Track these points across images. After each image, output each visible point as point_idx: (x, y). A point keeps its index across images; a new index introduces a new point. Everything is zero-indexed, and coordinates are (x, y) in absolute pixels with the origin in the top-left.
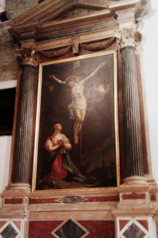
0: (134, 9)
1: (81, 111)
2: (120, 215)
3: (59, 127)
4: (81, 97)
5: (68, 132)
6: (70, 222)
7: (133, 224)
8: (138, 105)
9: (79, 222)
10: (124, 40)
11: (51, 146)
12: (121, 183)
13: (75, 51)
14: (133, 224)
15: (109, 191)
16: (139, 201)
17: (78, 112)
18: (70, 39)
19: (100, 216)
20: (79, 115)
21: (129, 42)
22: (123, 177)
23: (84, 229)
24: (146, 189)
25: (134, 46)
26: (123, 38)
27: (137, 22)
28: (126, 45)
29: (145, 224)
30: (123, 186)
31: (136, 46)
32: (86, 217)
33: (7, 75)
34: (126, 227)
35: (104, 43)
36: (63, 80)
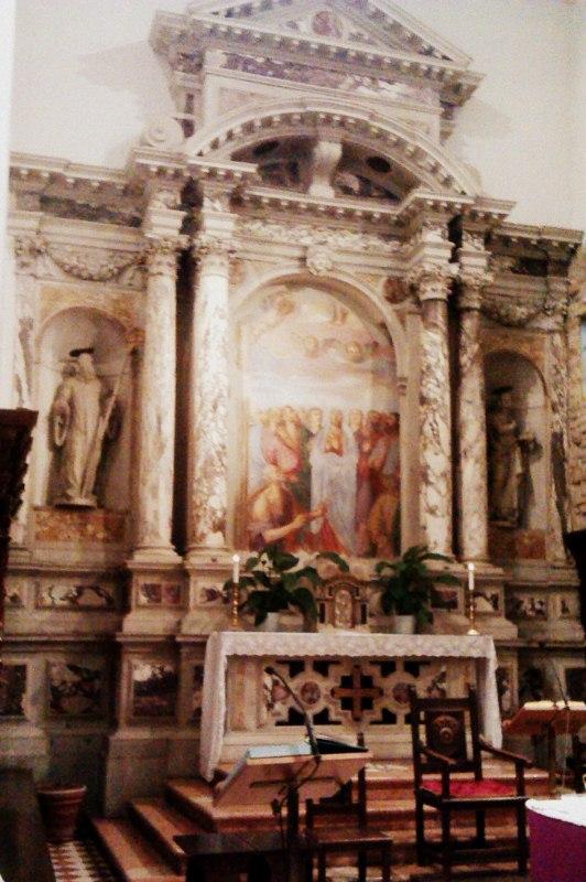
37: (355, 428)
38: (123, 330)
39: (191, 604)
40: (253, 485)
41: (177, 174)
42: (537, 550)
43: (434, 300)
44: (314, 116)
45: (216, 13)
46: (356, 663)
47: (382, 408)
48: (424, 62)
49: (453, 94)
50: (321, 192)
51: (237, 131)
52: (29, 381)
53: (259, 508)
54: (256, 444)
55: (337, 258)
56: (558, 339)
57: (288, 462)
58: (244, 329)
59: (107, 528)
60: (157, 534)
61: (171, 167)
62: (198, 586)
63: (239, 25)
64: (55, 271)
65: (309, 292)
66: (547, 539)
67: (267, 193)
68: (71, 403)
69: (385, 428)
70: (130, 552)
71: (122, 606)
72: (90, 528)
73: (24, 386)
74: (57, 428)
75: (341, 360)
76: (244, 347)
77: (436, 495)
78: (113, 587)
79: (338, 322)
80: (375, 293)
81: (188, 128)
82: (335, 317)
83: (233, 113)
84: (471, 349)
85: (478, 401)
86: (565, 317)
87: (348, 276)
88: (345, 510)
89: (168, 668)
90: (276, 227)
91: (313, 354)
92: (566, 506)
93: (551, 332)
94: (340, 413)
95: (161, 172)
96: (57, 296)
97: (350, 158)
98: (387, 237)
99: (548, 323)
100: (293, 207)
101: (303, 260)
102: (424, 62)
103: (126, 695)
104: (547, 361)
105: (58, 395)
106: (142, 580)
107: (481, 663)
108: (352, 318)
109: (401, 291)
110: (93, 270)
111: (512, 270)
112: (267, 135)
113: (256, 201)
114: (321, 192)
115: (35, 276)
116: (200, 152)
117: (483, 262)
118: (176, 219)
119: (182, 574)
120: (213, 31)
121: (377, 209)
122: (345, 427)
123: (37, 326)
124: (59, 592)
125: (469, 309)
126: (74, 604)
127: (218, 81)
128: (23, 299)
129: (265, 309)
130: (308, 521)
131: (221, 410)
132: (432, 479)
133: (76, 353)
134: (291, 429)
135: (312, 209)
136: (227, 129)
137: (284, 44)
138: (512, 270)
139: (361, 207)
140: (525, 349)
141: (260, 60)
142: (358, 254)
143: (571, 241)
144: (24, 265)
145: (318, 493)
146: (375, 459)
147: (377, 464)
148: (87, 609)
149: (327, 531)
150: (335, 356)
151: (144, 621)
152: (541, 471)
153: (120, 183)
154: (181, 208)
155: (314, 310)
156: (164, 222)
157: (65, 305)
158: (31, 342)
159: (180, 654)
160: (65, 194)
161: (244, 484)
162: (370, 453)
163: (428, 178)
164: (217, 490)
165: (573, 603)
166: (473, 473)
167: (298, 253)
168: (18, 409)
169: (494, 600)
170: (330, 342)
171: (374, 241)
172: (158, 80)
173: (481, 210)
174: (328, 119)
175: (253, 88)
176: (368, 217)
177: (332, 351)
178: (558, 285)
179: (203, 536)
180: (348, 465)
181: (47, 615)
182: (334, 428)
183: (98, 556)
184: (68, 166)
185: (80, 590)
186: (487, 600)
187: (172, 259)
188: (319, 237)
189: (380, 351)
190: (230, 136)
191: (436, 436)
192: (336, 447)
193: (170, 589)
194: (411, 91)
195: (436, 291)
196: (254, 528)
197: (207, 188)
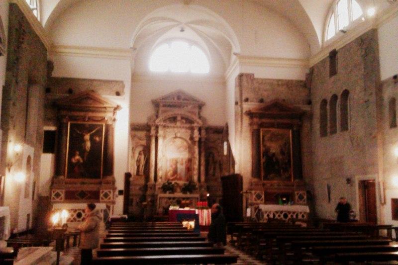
3: (78, 153)
5: (81, 155)
6: (82, 191)
7: (58, 192)
11: (74, 161)
12: (103, 178)
13: (87, 120)
14: (58, 192)
15: (98, 180)
17: (86, 147)
19: (95, 189)
20: (87, 149)
21: (110, 123)
22: (103, 175)
23: (77, 197)
27: (114, 113)
29: (110, 192)
32: (88, 189)
36: (80, 131)
46: (179, 198)
54: (168, 165)
57: (174, 166)
77: (196, 172)
87: (184, 137)
88: (183, 174)
91: (179, 148)
97: (182, 118)
105: (138, 157)
109: (192, 138)
114: (178, 124)
124: (138, 188)
151: (149, 192)
161: (166, 170)
166: (202, 168)
168: (352, 23)
174: (178, 114)
180: (184, 167)
195: (197, 139)
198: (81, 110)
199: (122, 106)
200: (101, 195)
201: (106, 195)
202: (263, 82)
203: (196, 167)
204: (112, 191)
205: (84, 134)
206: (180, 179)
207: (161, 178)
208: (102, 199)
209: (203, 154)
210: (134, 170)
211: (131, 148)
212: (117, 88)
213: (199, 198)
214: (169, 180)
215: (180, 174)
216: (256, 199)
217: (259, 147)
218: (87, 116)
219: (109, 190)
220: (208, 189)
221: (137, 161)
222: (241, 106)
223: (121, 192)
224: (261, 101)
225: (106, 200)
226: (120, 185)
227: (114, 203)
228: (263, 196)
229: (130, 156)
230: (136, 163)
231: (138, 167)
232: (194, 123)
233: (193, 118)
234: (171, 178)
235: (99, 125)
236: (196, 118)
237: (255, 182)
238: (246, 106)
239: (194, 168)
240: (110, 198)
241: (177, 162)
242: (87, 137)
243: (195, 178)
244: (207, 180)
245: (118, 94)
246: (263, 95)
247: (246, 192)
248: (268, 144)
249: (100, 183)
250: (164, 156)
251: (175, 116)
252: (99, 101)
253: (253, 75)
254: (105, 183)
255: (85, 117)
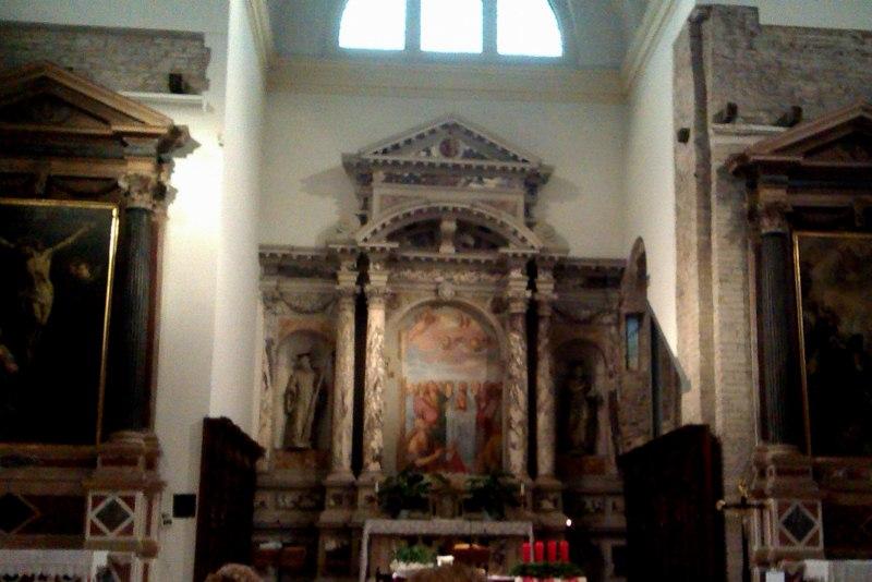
0: (157, 140)
1: (42, 306)
2: (93, 488)
4: (44, 280)
8: (146, 314)
9: (25, 496)
10: (135, 195)
13: (39, 189)
16: (127, 470)
17: (36, 307)
18: (31, 161)
19: (62, 489)
21: (142, 201)
24: (140, 452)
25: (149, 207)
26: (133, 189)
28: (137, 204)
29: (130, 501)
30: (106, 446)
31: (154, 206)
32: (37, 489)
33: (735, 271)
34: (101, 506)
35: (95, 187)
37: (475, 393)
38: (326, 340)
39: (359, 504)
40: (409, 428)
41: (353, 251)
42: (599, 469)
43: (518, 314)
44: (436, 209)
45: (376, 153)
47: (493, 380)
48: (510, 165)
49: (534, 181)
50: (447, 250)
51: (388, 223)
52: (271, 375)
53: (413, 446)
55: (459, 288)
56: (613, 330)
57: (431, 416)
58: (404, 335)
59: (317, 461)
60: (341, 465)
61: (349, 248)
62: (363, 494)
63: (390, 158)
64: (286, 309)
65: (446, 309)
66: (606, 461)
67: (411, 254)
68: (297, 386)
69: (493, 393)
70: (325, 475)
71: (321, 507)
72: (307, 461)
73: (268, 377)
74: (289, 402)
75: (465, 350)
76: (403, 346)
77: (516, 436)
78: (315, 495)
79: (464, 327)
80: (485, 309)
81: (364, 220)
82: (462, 324)
83: (386, 212)
84: (544, 343)
85: (547, 375)
86: (619, 315)
87: (467, 299)
88: (468, 445)
89: (346, 542)
90: (420, 272)
92: (619, 438)
93: (609, 325)
94: (466, 384)
95: (343, 251)
96: (288, 323)
97: (463, 227)
98: (492, 272)
99: (608, 319)
100: (429, 260)
101: (436, 291)
102: (510, 165)
103: (321, 559)
104: (607, 344)
106: (331, 492)
107: (526, 538)
108: (474, 323)
109: (500, 306)
110: (308, 306)
111: (582, 286)
112: (410, 221)
113: (406, 259)
114: (447, 250)
115: (275, 314)
116: (362, 236)
117: (551, 286)
118: (353, 277)
119: (353, 489)
120: (376, 162)
121: (483, 257)
122: (469, 393)
123: (277, 343)
124: (288, 499)
125: (542, 317)
126: (296, 506)
127: (380, 190)
128: (268, 327)
129: (416, 322)
130: (445, 452)
131: (379, 389)
132: (513, 426)
133: (300, 356)
134: (433, 395)
135: (441, 261)
136: (382, 222)
137: (420, 164)
138: (582, 286)
139: (472, 257)
140: (591, 337)
141: (406, 175)
142: (473, 285)
143: (619, 267)
144: (268, 308)
145: (451, 435)
146: (488, 413)
147: (489, 416)
148: (304, 509)
149: (456, 457)
150: (462, 348)
151: (332, 515)
152: (603, 416)
153: (324, 255)
154: (356, 270)
155: (448, 322)
156: (348, 279)
157: (293, 328)
158: (273, 353)
159: (350, 532)
160: (292, 264)
161: (403, 430)
162: (485, 408)
163: (512, 238)
164: (376, 437)
165: (620, 503)
166: (544, 420)
167: (433, 287)
169: (555, 502)
170: (459, 340)
171: (484, 276)
172: (350, 188)
173: (547, 255)
174: (445, 209)
175: (400, 193)
176: (477, 262)
177: (461, 345)
178: (614, 295)
179: (368, 465)
180: (471, 416)
181: (281, 513)
182: (461, 394)
183: (312, 477)
184: (292, 249)
185: (301, 498)
186: (550, 501)
187: (351, 300)
188: (448, 276)
189: (489, 348)
190: (384, 226)
191: (516, 399)
192: (462, 405)
193: (348, 496)
194: (505, 181)
195: (518, 308)
196: (409, 458)
197: (371, 257)
198: (58, 187)
199: (195, 134)
200: (91, 515)
201: (112, 517)
202: (799, 40)
203: (517, 415)
204: (139, 496)
205: (28, 249)
206: (457, 466)
207: (378, 459)
208: (95, 531)
209: (544, 365)
210: (273, 427)
211: (260, 346)
212: (178, 62)
213: (531, 533)
214: (412, 466)
215: (456, 445)
216: (789, 535)
217: (788, 313)
218: (43, 176)
219: (128, 493)
220: (571, 504)
221: (288, 392)
222: (702, 144)
223: (183, 506)
224: (793, 118)
225: (111, 536)
226: (181, 470)
227: (149, 551)
228: (819, 524)
229: (258, 374)
230: (280, 401)
231: (291, 417)
232: (505, 243)
233: (503, 225)
234: (421, 462)
235: (91, 215)
236: (515, 223)
237: (775, 460)
238: (724, 143)
239: (510, 419)
240: (129, 530)
241: (442, 399)
242: (41, 262)
243: (517, 458)
244: (559, 469)
245: (177, 85)
246: (797, 94)
247: (743, 505)
248: (828, 297)
249: (89, 464)
250: (391, 375)
251: (434, 216)
252: (101, 113)
253: (755, 10)
254: (105, 463)
255: (33, 178)
